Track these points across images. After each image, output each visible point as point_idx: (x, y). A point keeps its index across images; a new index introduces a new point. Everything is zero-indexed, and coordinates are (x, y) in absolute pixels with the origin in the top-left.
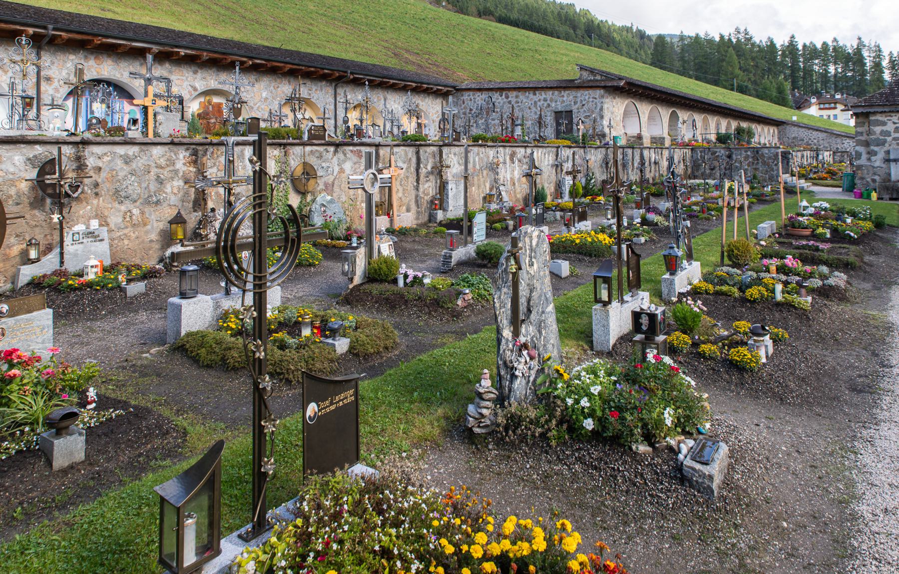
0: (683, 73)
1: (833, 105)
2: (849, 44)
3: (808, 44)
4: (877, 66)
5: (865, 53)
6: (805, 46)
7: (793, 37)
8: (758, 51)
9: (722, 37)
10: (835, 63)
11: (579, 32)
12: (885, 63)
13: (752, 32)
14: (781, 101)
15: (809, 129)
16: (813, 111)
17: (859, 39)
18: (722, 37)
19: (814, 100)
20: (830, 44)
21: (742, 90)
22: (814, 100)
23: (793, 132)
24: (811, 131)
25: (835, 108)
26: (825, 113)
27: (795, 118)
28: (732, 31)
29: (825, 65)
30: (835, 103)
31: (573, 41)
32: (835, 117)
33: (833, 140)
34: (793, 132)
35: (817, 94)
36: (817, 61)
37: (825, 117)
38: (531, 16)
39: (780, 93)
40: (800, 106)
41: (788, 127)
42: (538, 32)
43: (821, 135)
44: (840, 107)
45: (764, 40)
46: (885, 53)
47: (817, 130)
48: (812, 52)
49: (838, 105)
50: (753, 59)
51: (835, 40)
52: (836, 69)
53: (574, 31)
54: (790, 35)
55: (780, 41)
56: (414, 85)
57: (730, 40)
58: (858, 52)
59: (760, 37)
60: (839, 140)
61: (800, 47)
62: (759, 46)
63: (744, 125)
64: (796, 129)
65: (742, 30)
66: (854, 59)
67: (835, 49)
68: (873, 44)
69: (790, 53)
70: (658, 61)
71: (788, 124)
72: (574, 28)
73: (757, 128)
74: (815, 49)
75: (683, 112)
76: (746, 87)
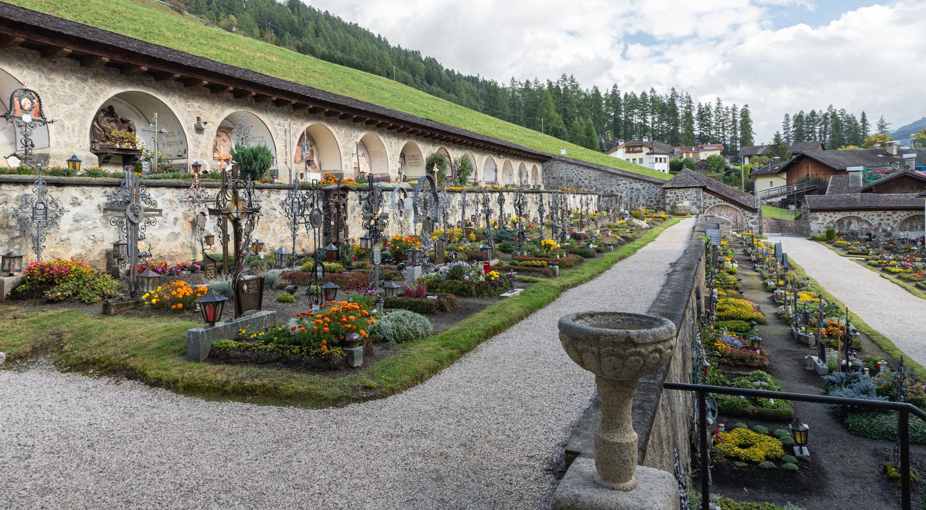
0: (514, 120)
1: (638, 149)
2: (663, 93)
3: (629, 94)
4: (688, 115)
5: (678, 104)
6: (626, 96)
7: (615, 86)
8: (584, 100)
9: (550, 84)
10: (653, 113)
11: (418, 78)
12: (695, 114)
13: (577, 79)
14: (589, 144)
15: (580, 165)
16: (620, 154)
17: (673, 89)
18: (550, 84)
19: (621, 143)
20: (648, 94)
21: (557, 134)
22: (621, 143)
23: (562, 170)
24: (581, 169)
25: (641, 151)
26: (631, 156)
27: (563, 152)
28: (560, 77)
29: (643, 115)
30: (641, 146)
31: (411, 86)
32: (641, 160)
33: (607, 180)
34: (562, 170)
35: (627, 137)
36: (636, 111)
37: (631, 161)
38: (367, 58)
39: (588, 135)
40: (609, 148)
41: (555, 164)
42: (342, 64)
43: (593, 174)
44: (646, 150)
45: (591, 89)
46: (695, 105)
47: (589, 167)
48: (633, 103)
49: (644, 149)
50: (579, 106)
51: (653, 90)
52: (653, 119)
53: (414, 76)
54: (613, 84)
55: (605, 89)
56: (779, 199)
57: (558, 87)
58: (672, 100)
59: (586, 87)
60: (614, 181)
61: (622, 96)
62: (585, 95)
63: (456, 155)
64: (564, 166)
65: (568, 77)
66: (666, 109)
67: (652, 99)
68: (685, 95)
69: (613, 102)
70: (490, 107)
71: (555, 160)
72: (414, 74)
73: (479, 161)
74: (636, 98)
75: (394, 140)
76: (561, 130)
